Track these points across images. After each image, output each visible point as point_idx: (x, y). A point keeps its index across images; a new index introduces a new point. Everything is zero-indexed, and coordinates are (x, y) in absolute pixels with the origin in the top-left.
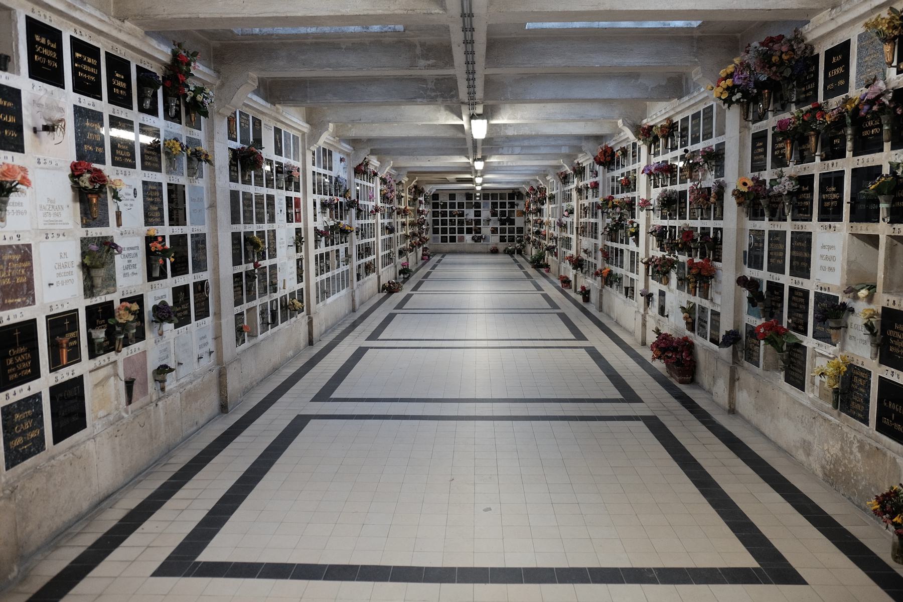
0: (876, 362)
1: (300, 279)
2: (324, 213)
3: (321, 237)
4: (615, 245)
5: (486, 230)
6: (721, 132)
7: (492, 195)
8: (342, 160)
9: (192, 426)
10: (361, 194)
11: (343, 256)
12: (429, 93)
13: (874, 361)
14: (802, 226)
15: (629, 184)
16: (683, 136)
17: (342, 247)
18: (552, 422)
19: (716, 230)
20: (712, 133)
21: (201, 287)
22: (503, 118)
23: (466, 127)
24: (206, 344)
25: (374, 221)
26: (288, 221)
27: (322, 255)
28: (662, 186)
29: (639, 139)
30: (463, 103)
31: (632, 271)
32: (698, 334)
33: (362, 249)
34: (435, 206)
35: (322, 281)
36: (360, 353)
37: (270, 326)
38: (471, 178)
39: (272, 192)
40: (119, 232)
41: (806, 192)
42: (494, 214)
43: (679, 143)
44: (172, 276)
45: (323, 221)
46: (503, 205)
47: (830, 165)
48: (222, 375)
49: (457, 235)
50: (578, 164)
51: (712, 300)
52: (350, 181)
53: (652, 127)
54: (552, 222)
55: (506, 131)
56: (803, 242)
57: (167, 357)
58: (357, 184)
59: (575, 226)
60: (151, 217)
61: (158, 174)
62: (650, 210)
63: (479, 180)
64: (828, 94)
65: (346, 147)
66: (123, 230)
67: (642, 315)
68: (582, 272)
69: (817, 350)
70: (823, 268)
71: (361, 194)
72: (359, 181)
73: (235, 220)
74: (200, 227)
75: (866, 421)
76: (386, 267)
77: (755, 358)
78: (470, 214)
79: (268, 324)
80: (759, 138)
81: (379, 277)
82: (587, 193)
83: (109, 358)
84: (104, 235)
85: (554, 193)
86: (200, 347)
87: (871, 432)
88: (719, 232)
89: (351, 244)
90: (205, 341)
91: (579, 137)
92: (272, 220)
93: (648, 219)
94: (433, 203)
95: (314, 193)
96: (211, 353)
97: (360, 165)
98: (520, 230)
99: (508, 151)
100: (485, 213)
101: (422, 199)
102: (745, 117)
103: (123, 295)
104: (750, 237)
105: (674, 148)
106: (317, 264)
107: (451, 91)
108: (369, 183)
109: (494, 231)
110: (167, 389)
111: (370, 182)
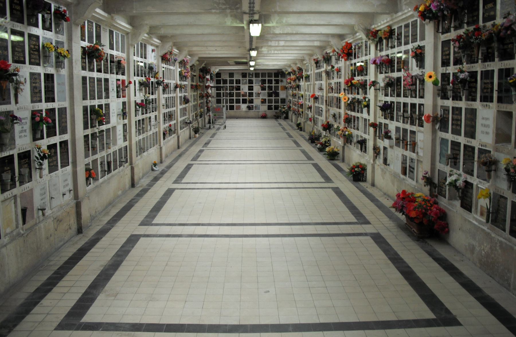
0: (510, 191)
1: (125, 140)
2: (140, 90)
3: (139, 108)
4: (353, 114)
5: (257, 101)
6: (423, 38)
7: (262, 74)
8: (153, 51)
9: (61, 241)
10: (166, 74)
11: (153, 121)
12: (221, 6)
13: (509, 191)
14: (471, 105)
15: (362, 71)
16: (399, 39)
17: (152, 115)
18: (309, 238)
19: (420, 105)
20: (417, 38)
21: (64, 144)
22: (272, 22)
23: (246, 27)
24: (67, 185)
25: (175, 95)
26: (118, 97)
27: (139, 121)
28: (386, 73)
29: (369, 39)
30: (245, 13)
31: (365, 133)
32: (409, 177)
33: (167, 116)
34: (218, 82)
35: (140, 141)
36: (169, 192)
37: (106, 172)
38: (247, 62)
39: (108, 76)
40: (16, 108)
41: (473, 82)
42: (263, 89)
43: (396, 43)
44: (47, 137)
45: (139, 97)
46: (270, 82)
47: (487, 66)
48: (78, 206)
49: (235, 104)
50: (327, 53)
51: (417, 153)
52: (158, 66)
53: (378, 31)
54: (308, 96)
55: (275, 31)
56: (472, 113)
57: (45, 193)
58: (163, 67)
59: (325, 99)
60: (35, 97)
61: (38, 67)
62: (377, 89)
63: (252, 63)
64: (485, 20)
65: (156, 41)
66: (19, 107)
67: (372, 164)
68: (330, 133)
69: (479, 186)
70: (482, 132)
71: (166, 74)
72: (165, 66)
73: (85, 98)
74: (63, 103)
75: (504, 230)
76: (183, 130)
77: (444, 193)
78: (245, 88)
79: (105, 171)
80: (446, 44)
81: (178, 137)
82: (333, 74)
83: (12, 193)
84: (8, 110)
85: (308, 73)
86: (64, 187)
87: (507, 236)
88: (422, 106)
89: (159, 113)
90: (67, 183)
91: (327, 35)
92: (107, 97)
93: (376, 96)
94: (217, 80)
95: (135, 76)
96: (70, 191)
97: (166, 54)
98: (283, 101)
99: (275, 44)
100: (257, 88)
101: (208, 77)
102: (437, 31)
103: (19, 150)
104: (441, 110)
105: (393, 47)
106: (136, 128)
107: (237, 4)
108: (169, 66)
109: (263, 101)
110: (46, 214)
111: (170, 65)
